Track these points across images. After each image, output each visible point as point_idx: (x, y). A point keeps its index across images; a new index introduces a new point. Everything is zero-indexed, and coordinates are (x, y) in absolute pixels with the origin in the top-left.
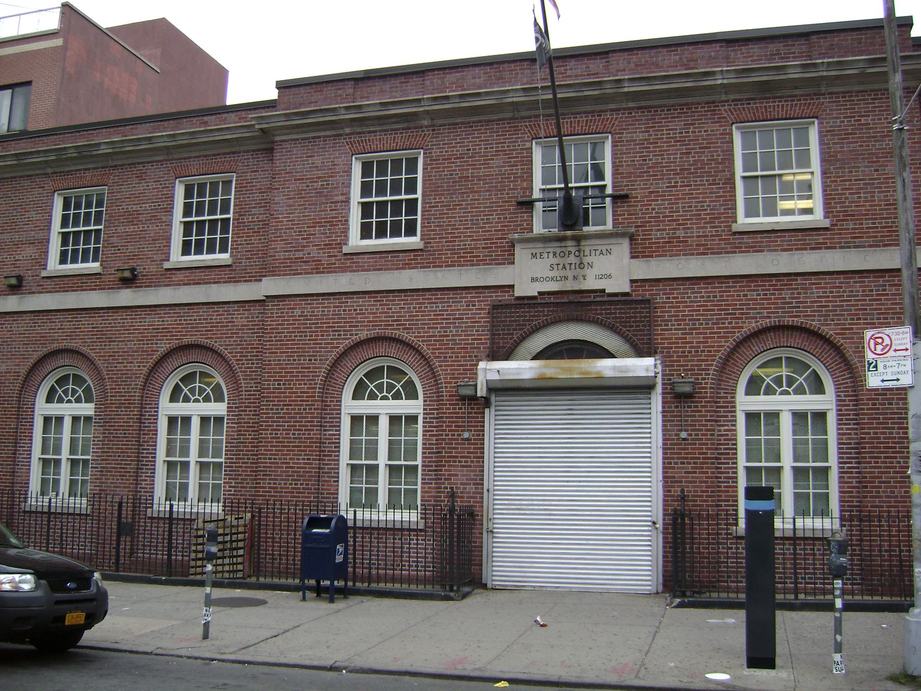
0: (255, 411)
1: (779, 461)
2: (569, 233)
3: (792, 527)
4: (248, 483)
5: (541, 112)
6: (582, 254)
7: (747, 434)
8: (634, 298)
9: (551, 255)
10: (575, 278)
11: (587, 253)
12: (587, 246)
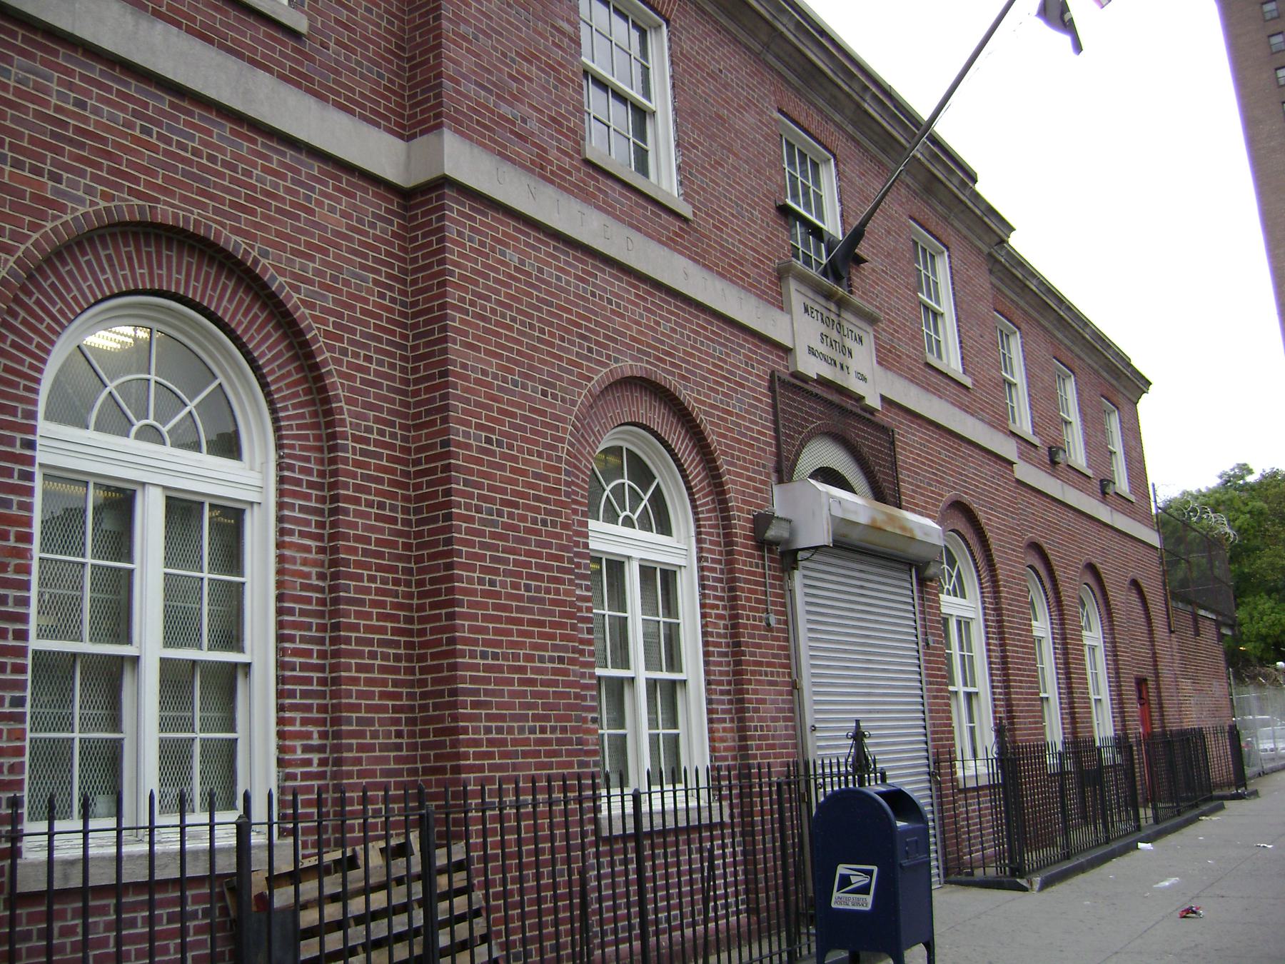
0: (381, 506)
1: (128, 640)
3: (43, 856)
4: (375, 735)
7: (169, 561)
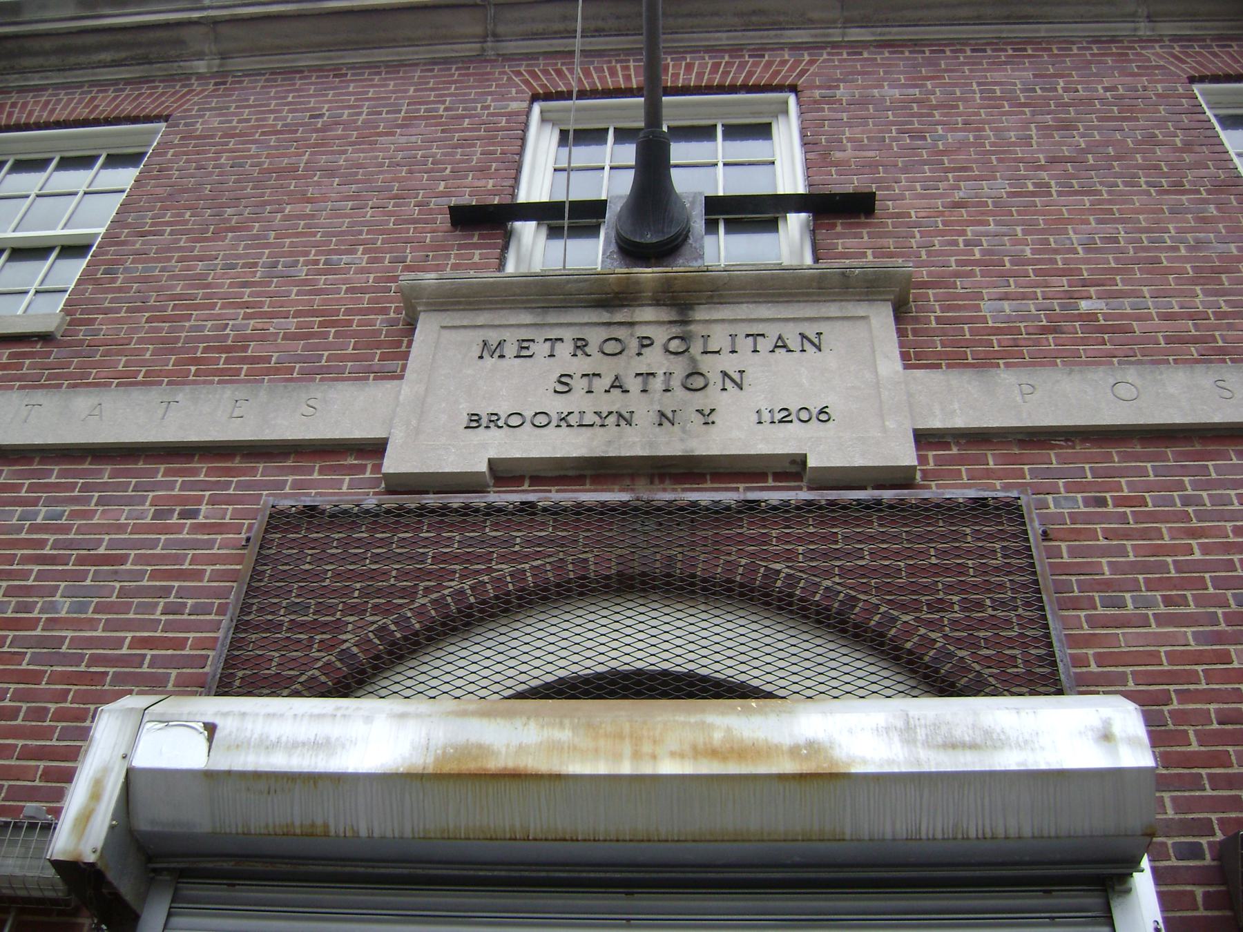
2: (647, 274)
5: (578, 43)
6: (696, 348)
8: (934, 492)
9: (565, 350)
10: (663, 418)
11: (719, 338)
12: (717, 326)
